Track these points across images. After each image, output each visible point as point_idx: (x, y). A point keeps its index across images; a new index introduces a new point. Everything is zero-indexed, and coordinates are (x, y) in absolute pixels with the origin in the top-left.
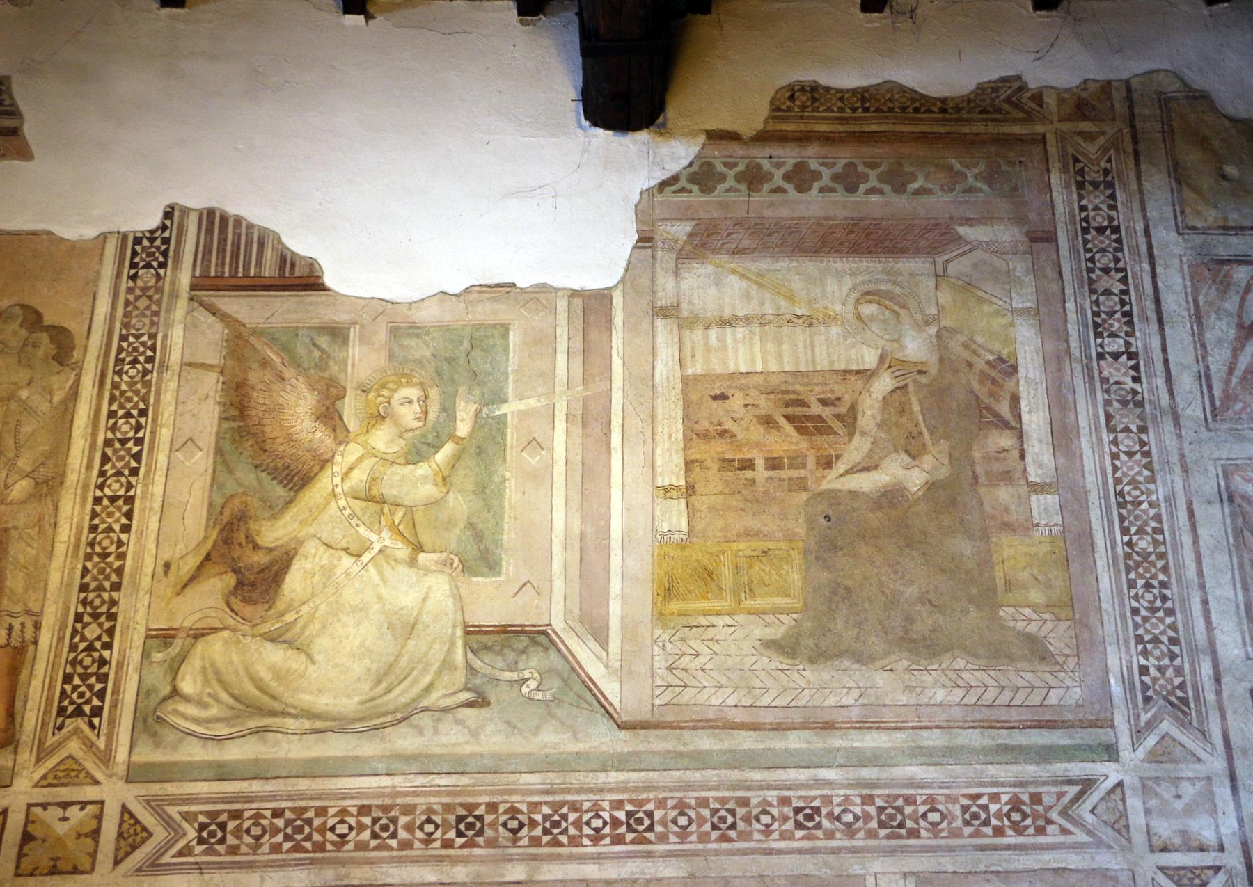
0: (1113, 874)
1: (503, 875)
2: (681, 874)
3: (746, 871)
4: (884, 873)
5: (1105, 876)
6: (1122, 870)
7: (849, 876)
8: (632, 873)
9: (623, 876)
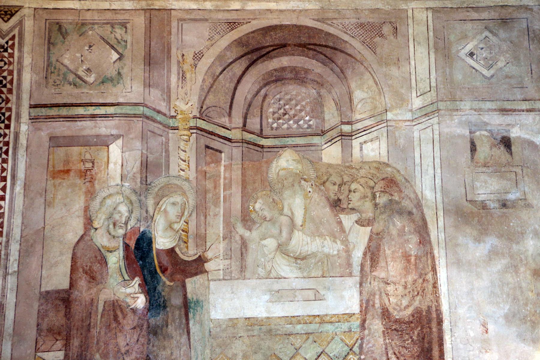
0: (530, 7)
1: (229, 7)
2: (317, 8)
3: (349, 7)
4: (417, 8)
5: (526, 8)
6: (535, 5)
7: (399, 10)
8: (293, 7)
9: (289, 8)
